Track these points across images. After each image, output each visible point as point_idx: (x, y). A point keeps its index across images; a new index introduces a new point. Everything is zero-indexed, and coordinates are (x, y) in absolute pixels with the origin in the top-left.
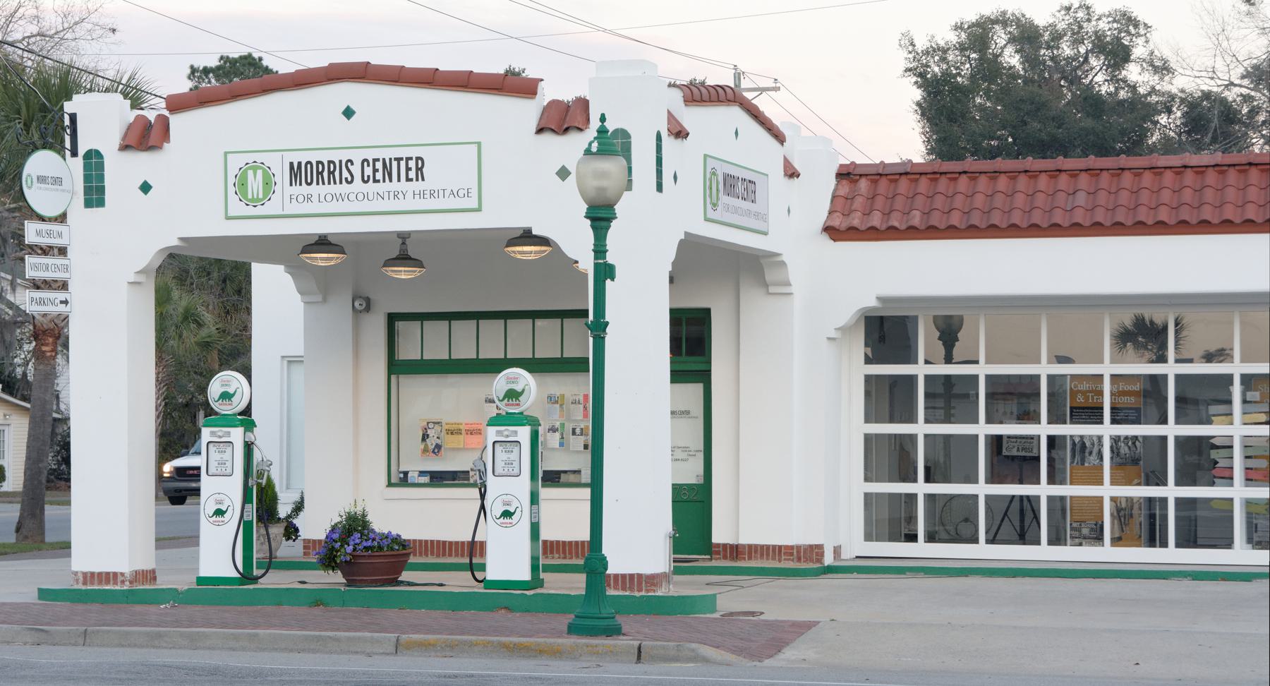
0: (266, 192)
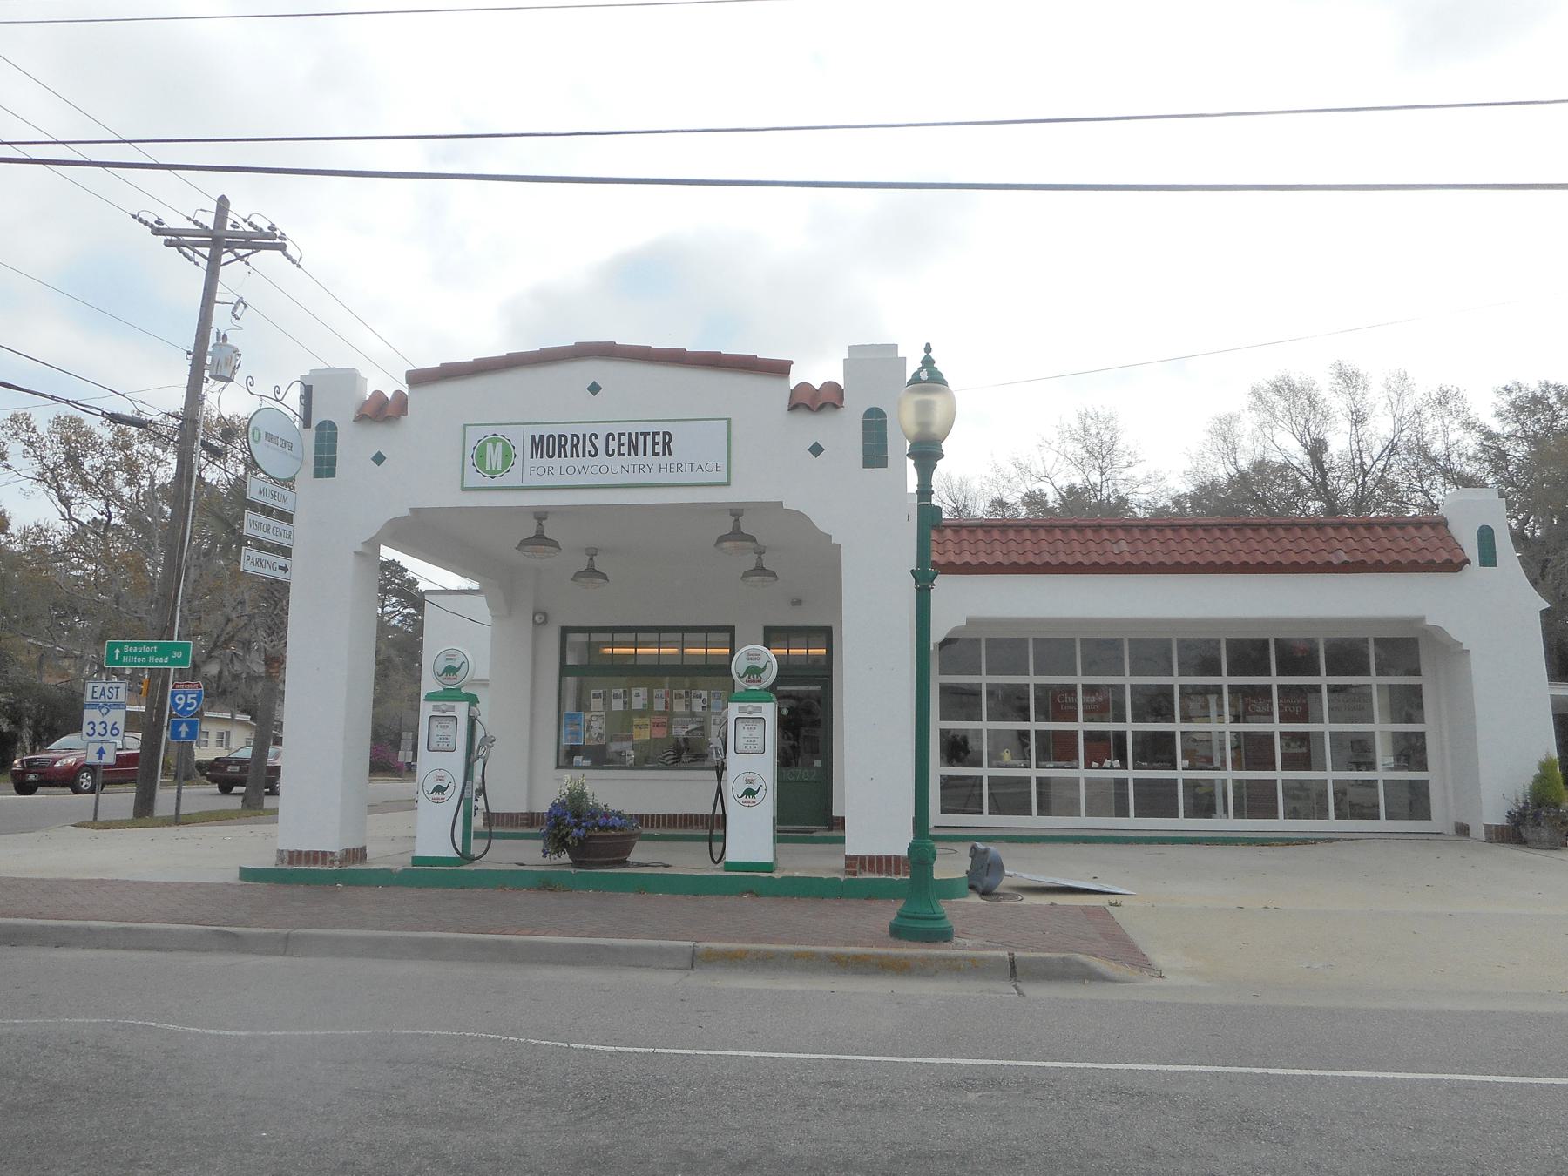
0: (505, 465)
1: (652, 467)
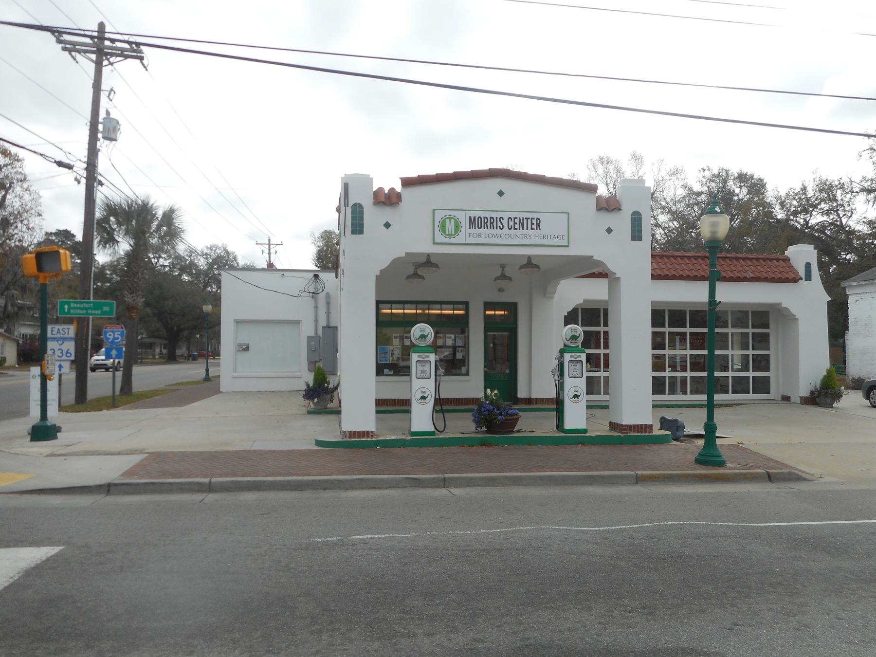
1: (529, 236)
